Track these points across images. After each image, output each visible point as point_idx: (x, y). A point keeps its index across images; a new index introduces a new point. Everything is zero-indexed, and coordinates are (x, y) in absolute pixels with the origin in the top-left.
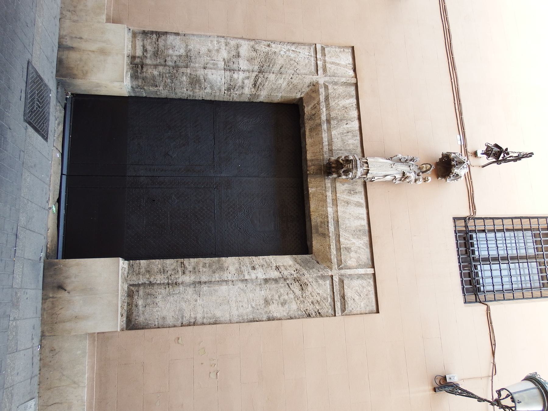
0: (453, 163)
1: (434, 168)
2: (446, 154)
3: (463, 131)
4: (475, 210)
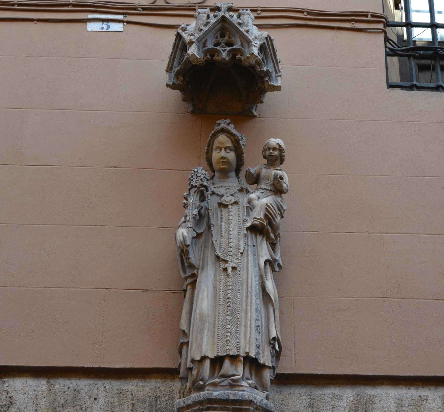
0: (224, 55)
1: (228, 121)
2: (177, 75)
3: (70, 8)
4: (366, 16)
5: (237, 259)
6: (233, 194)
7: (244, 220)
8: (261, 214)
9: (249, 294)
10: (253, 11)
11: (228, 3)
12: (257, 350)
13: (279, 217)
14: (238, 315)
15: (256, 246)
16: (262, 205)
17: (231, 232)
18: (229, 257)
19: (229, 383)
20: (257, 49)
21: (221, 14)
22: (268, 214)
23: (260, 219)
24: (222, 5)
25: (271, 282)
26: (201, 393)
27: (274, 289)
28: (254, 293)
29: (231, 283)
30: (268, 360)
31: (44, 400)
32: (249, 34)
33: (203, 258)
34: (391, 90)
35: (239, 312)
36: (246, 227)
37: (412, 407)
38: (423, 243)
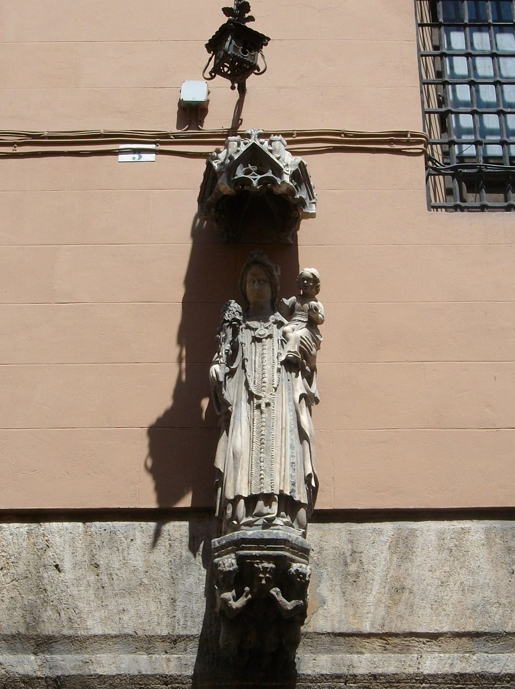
5: (271, 394)
6: (267, 327)
7: (278, 354)
8: (295, 348)
9: (284, 431)
10: (285, 135)
11: (259, 130)
12: (292, 488)
13: (314, 349)
14: (272, 452)
15: (290, 381)
16: (297, 338)
17: (265, 367)
18: (262, 392)
19: (264, 522)
20: (289, 176)
21: (251, 141)
22: (302, 346)
23: (295, 352)
24: (252, 131)
25: (307, 417)
26: (235, 533)
27: (310, 424)
28: (288, 428)
29: (264, 420)
30: (303, 497)
31: (81, 543)
32: (280, 161)
33: (237, 395)
34: (433, 212)
35: (273, 449)
36: (280, 360)
37: (454, 540)
38: (465, 370)
